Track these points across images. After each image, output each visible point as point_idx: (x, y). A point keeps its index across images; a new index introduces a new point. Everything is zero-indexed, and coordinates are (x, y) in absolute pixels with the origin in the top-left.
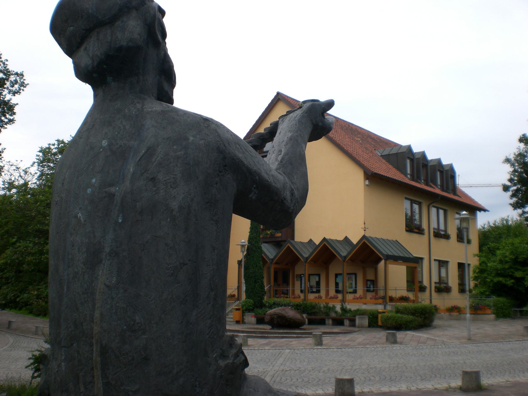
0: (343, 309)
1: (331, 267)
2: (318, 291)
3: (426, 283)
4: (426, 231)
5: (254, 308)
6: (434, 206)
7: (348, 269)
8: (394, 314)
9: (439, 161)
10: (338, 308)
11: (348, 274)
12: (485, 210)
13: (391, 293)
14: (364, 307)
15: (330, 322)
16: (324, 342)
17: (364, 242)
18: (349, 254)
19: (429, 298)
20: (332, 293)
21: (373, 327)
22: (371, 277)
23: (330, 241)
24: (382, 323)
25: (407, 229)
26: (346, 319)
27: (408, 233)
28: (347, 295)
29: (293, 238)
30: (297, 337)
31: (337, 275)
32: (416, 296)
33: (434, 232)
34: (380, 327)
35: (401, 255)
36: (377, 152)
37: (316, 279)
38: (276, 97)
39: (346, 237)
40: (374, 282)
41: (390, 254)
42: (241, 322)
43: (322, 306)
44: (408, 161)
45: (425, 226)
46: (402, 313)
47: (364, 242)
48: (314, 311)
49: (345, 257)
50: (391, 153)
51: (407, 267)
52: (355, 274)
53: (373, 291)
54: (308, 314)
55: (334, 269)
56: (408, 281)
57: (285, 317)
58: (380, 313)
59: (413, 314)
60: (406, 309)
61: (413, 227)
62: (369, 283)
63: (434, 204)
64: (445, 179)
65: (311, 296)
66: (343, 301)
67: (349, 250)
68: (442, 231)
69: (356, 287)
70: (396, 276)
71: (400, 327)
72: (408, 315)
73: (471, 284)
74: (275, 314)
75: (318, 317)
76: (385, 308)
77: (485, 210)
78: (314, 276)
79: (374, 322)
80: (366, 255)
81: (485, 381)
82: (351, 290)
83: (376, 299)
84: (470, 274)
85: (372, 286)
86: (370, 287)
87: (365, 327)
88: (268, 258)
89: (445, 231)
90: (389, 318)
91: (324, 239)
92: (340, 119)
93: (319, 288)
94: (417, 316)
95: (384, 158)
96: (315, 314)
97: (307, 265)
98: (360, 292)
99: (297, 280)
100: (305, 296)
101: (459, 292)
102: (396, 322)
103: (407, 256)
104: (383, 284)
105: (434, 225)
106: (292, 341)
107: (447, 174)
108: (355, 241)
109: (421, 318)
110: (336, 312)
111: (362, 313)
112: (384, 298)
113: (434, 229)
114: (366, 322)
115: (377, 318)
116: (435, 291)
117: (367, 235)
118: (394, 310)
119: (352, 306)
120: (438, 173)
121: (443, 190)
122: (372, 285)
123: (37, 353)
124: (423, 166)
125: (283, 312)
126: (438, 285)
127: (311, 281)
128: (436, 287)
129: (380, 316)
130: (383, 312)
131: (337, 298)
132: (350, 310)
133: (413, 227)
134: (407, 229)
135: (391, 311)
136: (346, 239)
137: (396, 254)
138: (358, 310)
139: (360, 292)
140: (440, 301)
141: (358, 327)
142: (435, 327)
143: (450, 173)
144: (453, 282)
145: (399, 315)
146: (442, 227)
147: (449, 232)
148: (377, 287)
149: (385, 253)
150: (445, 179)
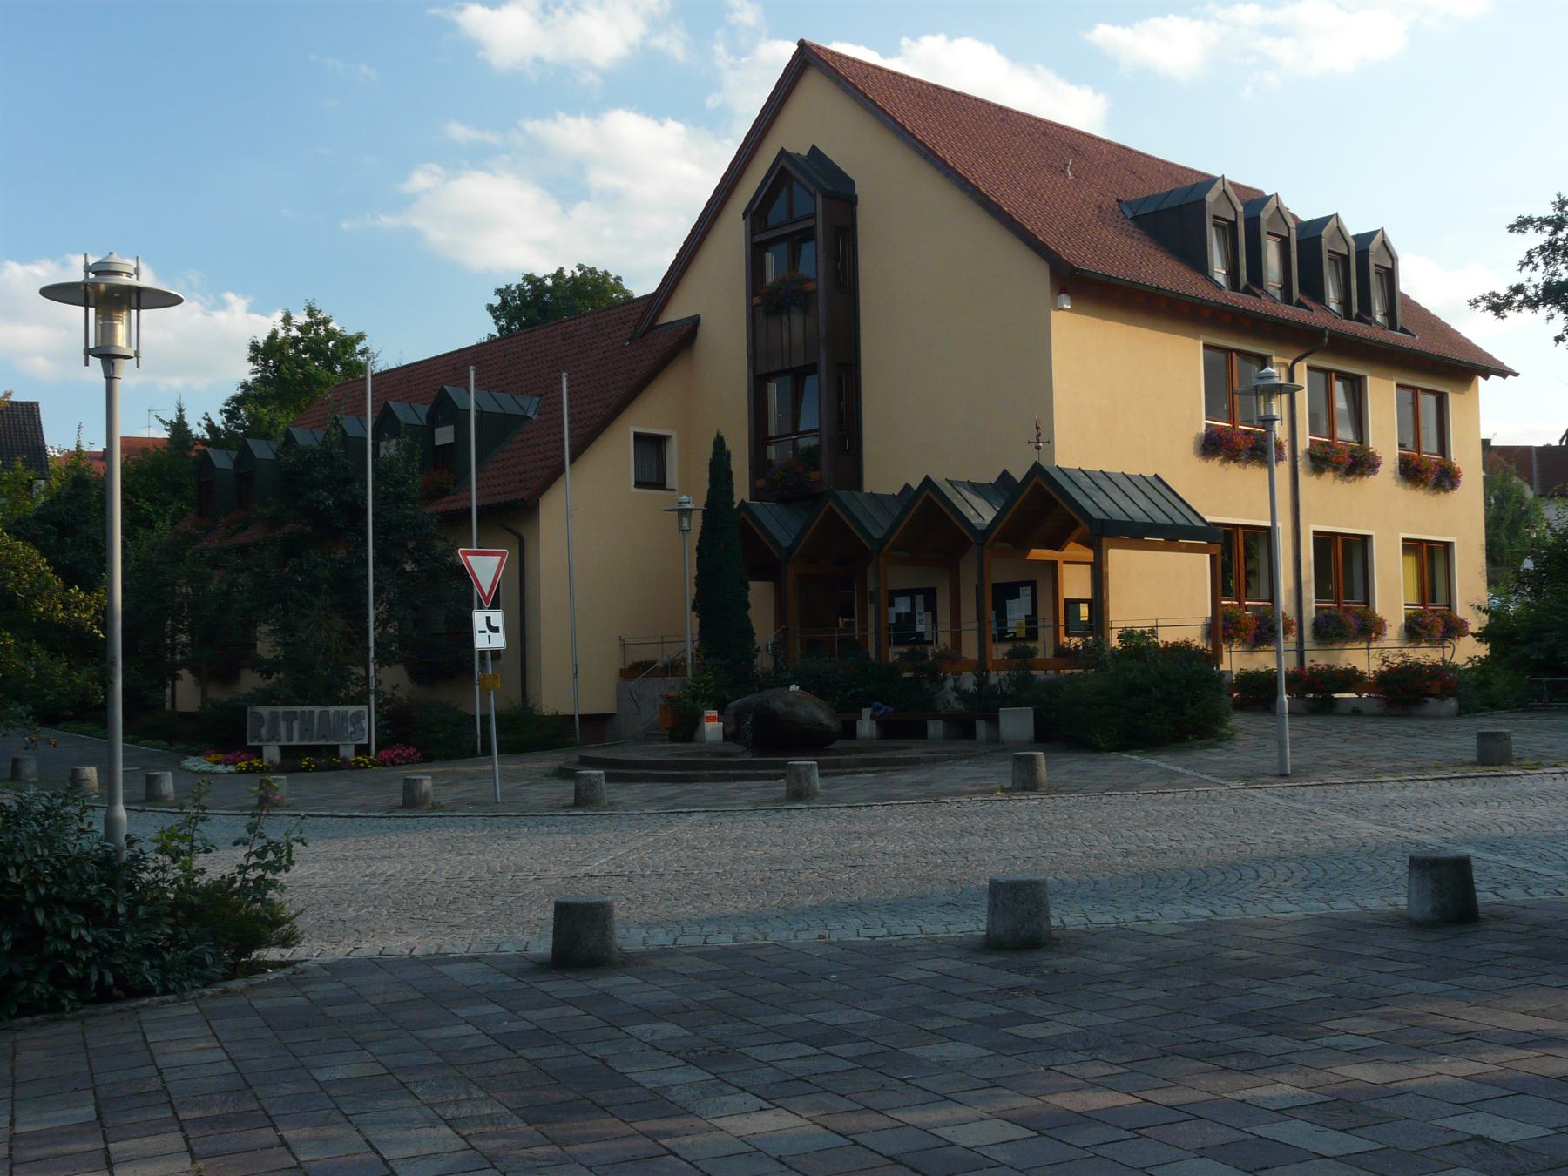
12: (1504, 372)
35: (1161, 518)
38: (797, 56)
50: (1164, 207)
52: (1033, 584)
77: (1504, 372)
81: (1064, 916)
92: (1012, 111)
107: (1367, 265)
137: (1139, 516)
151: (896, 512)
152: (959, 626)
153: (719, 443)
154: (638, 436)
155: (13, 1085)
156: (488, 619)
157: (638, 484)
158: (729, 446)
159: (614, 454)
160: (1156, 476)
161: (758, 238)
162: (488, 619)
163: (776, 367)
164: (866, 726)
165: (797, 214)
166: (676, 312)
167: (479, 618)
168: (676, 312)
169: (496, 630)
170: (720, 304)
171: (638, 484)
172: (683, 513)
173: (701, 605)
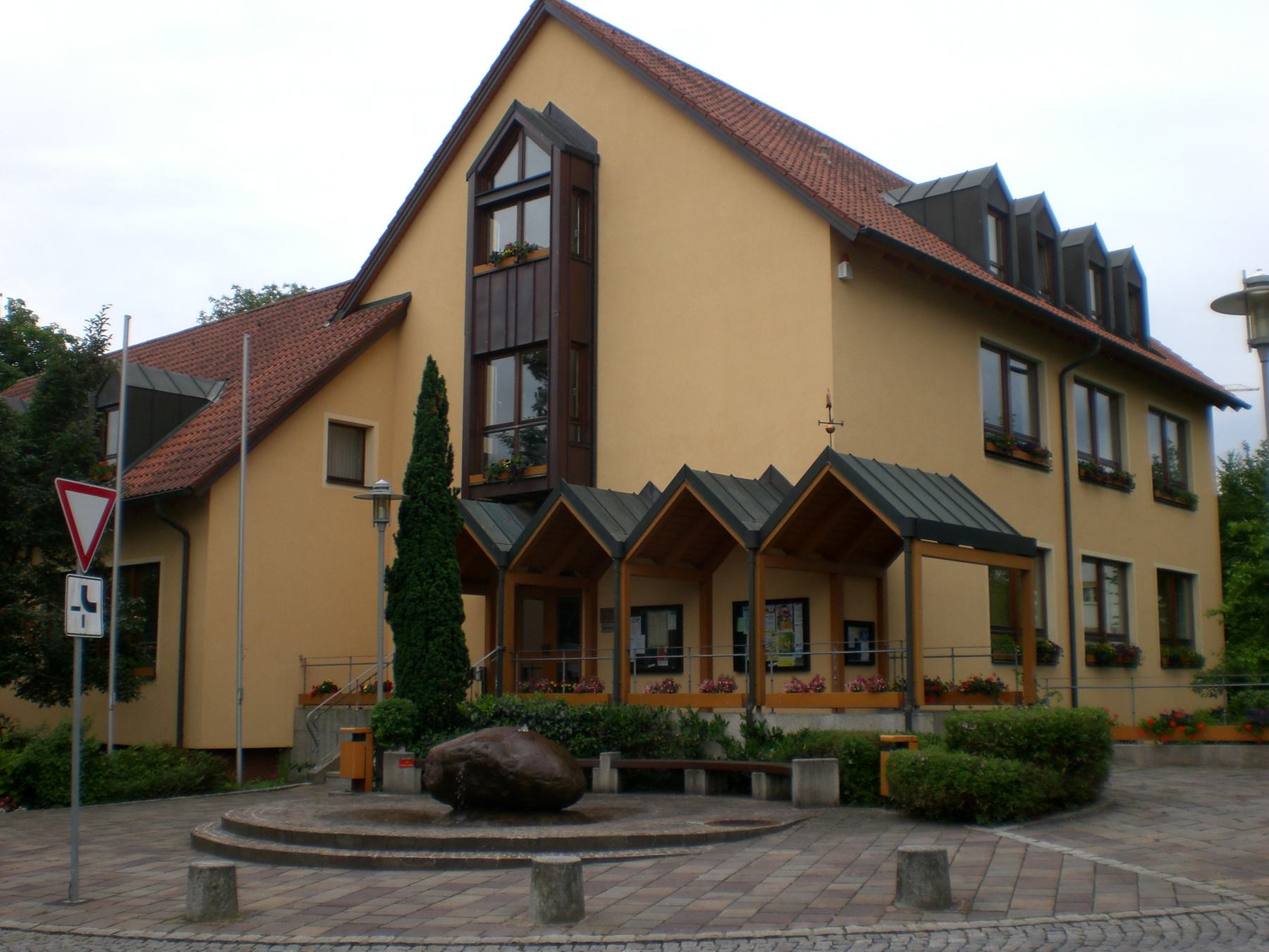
0: (753, 732)
1: (717, 577)
2: (677, 667)
3: (1056, 634)
4: (1055, 461)
5: (419, 732)
6: (1079, 381)
7: (775, 582)
8: (937, 752)
9: (1091, 237)
10: (735, 729)
11: (769, 602)
13: (933, 669)
14: (829, 722)
15: (702, 780)
16: (591, 902)
17: (829, 476)
18: (774, 519)
19: (1067, 683)
20: (723, 665)
21: (860, 802)
22: (860, 610)
23: (708, 483)
24: (893, 789)
25: (991, 447)
26: (759, 769)
27: (991, 461)
28: (768, 678)
29: (589, 477)
30: (505, 864)
31: (738, 608)
32: (1030, 682)
33: (1080, 465)
34: (887, 803)
35: (969, 523)
36: (884, 196)
37: (663, 625)
39: (771, 467)
40: (874, 630)
41: (925, 515)
42: (370, 783)
43: (676, 718)
44: (991, 221)
45: (1050, 440)
46: (974, 748)
47: (829, 476)
48: (646, 737)
49: (759, 536)
50: (931, 194)
51: (992, 569)
52: (805, 603)
53: (870, 663)
54: (623, 750)
55: (728, 587)
56: (994, 629)
57: (497, 766)
58: (887, 746)
59: (1022, 753)
60: (991, 729)
61: (1006, 446)
62: (853, 633)
63: (1074, 372)
64: (1111, 299)
65: (641, 686)
66: (754, 699)
67: (773, 506)
68: (1107, 463)
69: (806, 648)
70: (950, 602)
71: (961, 808)
72: (999, 755)
73: (1207, 638)
74: (462, 756)
75: (664, 761)
76: (909, 725)
78: (663, 613)
79: (864, 781)
80: (841, 529)
82: (790, 661)
83: (874, 690)
84: (1207, 599)
85: (864, 645)
86: (858, 647)
87: (826, 805)
88: (496, 551)
89: (1117, 464)
90: (919, 770)
91: (685, 473)
93: (680, 652)
94: (1041, 762)
95: (904, 212)
96: (649, 748)
97: (624, 568)
98: (822, 665)
99: (605, 629)
100: (753, 685)
101: (1163, 666)
102: (949, 787)
103: (990, 528)
104: (902, 635)
105: (1078, 444)
106: (463, 889)
107: (1122, 283)
108: (793, 477)
109: (1057, 767)
110: (727, 743)
111: (812, 746)
112: (906, 688)
113: (1080, 454)
114: (831, 784)
115: (876, 765)
116: (1088, 664)
117: (841, 449)
118: (943, 733)
119: (784, 721)
120: (1091, 274)
121: (1106, 326)
122: (865, 643)
123: (995, 680)
124: (1040, 246)
125: (492, 750)
126: (1095, 644)
127: (650, 631)
128: (1088, 651)
129: (885, 756)
130: (902, 745)
131: (732, 688)
132: (779, 735)
133: (1006, 446)
134: (991, 447)
135: (932, 740)
136: (771, 472)
138: (805, 734)
139: (822, 665)
140: (1100, 695)
141: (800, 805)
142: (1114, 807)
143: (1126, 279)
144: (1144, 632)
145: (963, 756)
146: (1105, 453)
147: (1129, 467)
148: (881, 646)
149: (907, 514)
150: (1111, 299)
151: (640, 515)
152: (710, 651)
153: (432, 367)
154: (333, 424)
155: (953, 656)
156: (85, 589)
157: (332, 479)
158: (442, 372)
159: (308, 444)
160: (951, 476)
161: (483, 202)
162: (85, 589)
163: (498, 346)
164: (605, 773)
165: (529, 175)
166: (387, 289)
167: (74, 585)
168: (387, 289)
169: (91, 607)
170: (436, 288)
171: (332, 479)
172: (381, 501)
173: (396, 614)
